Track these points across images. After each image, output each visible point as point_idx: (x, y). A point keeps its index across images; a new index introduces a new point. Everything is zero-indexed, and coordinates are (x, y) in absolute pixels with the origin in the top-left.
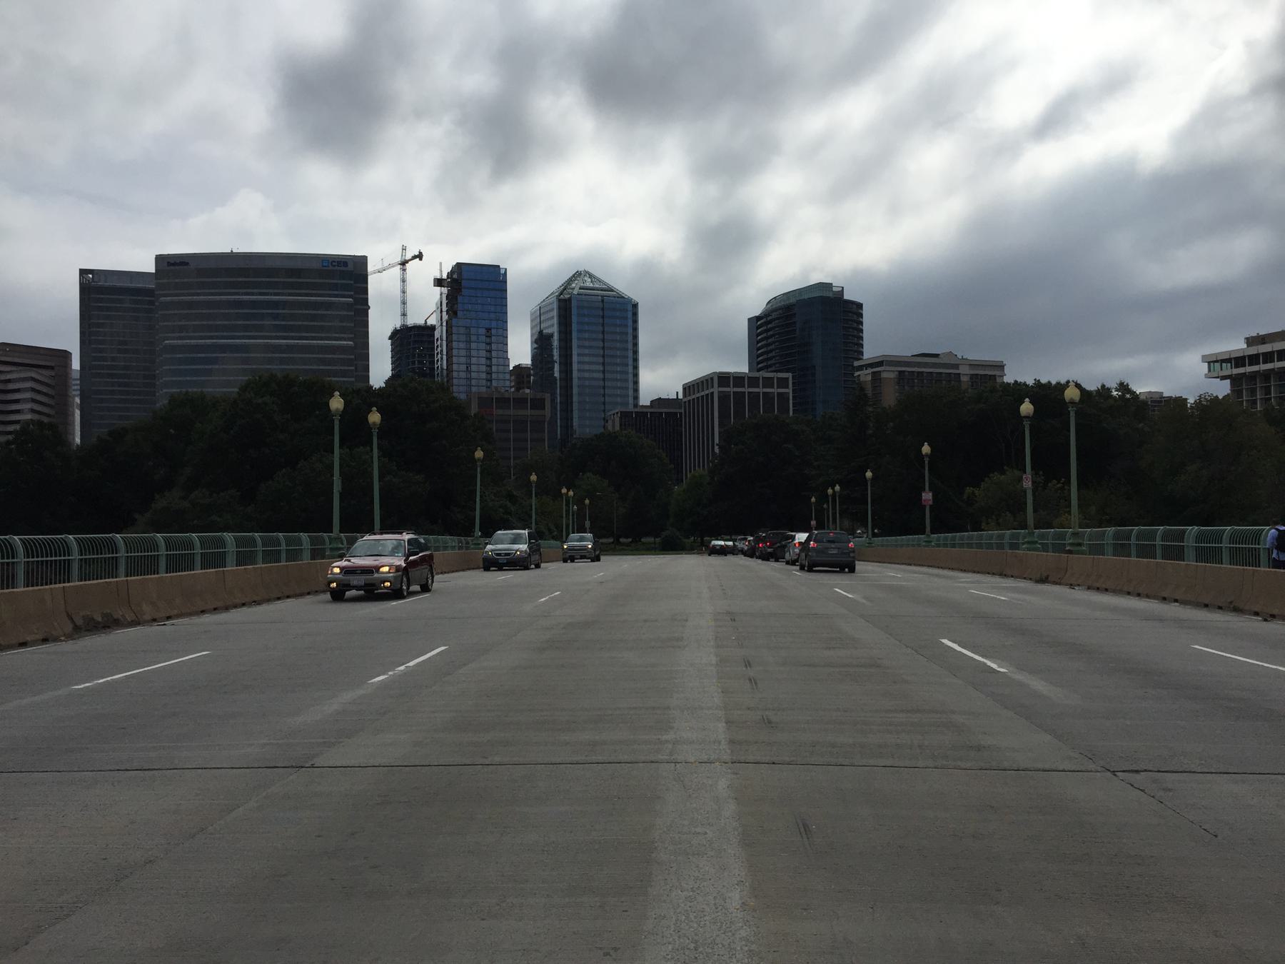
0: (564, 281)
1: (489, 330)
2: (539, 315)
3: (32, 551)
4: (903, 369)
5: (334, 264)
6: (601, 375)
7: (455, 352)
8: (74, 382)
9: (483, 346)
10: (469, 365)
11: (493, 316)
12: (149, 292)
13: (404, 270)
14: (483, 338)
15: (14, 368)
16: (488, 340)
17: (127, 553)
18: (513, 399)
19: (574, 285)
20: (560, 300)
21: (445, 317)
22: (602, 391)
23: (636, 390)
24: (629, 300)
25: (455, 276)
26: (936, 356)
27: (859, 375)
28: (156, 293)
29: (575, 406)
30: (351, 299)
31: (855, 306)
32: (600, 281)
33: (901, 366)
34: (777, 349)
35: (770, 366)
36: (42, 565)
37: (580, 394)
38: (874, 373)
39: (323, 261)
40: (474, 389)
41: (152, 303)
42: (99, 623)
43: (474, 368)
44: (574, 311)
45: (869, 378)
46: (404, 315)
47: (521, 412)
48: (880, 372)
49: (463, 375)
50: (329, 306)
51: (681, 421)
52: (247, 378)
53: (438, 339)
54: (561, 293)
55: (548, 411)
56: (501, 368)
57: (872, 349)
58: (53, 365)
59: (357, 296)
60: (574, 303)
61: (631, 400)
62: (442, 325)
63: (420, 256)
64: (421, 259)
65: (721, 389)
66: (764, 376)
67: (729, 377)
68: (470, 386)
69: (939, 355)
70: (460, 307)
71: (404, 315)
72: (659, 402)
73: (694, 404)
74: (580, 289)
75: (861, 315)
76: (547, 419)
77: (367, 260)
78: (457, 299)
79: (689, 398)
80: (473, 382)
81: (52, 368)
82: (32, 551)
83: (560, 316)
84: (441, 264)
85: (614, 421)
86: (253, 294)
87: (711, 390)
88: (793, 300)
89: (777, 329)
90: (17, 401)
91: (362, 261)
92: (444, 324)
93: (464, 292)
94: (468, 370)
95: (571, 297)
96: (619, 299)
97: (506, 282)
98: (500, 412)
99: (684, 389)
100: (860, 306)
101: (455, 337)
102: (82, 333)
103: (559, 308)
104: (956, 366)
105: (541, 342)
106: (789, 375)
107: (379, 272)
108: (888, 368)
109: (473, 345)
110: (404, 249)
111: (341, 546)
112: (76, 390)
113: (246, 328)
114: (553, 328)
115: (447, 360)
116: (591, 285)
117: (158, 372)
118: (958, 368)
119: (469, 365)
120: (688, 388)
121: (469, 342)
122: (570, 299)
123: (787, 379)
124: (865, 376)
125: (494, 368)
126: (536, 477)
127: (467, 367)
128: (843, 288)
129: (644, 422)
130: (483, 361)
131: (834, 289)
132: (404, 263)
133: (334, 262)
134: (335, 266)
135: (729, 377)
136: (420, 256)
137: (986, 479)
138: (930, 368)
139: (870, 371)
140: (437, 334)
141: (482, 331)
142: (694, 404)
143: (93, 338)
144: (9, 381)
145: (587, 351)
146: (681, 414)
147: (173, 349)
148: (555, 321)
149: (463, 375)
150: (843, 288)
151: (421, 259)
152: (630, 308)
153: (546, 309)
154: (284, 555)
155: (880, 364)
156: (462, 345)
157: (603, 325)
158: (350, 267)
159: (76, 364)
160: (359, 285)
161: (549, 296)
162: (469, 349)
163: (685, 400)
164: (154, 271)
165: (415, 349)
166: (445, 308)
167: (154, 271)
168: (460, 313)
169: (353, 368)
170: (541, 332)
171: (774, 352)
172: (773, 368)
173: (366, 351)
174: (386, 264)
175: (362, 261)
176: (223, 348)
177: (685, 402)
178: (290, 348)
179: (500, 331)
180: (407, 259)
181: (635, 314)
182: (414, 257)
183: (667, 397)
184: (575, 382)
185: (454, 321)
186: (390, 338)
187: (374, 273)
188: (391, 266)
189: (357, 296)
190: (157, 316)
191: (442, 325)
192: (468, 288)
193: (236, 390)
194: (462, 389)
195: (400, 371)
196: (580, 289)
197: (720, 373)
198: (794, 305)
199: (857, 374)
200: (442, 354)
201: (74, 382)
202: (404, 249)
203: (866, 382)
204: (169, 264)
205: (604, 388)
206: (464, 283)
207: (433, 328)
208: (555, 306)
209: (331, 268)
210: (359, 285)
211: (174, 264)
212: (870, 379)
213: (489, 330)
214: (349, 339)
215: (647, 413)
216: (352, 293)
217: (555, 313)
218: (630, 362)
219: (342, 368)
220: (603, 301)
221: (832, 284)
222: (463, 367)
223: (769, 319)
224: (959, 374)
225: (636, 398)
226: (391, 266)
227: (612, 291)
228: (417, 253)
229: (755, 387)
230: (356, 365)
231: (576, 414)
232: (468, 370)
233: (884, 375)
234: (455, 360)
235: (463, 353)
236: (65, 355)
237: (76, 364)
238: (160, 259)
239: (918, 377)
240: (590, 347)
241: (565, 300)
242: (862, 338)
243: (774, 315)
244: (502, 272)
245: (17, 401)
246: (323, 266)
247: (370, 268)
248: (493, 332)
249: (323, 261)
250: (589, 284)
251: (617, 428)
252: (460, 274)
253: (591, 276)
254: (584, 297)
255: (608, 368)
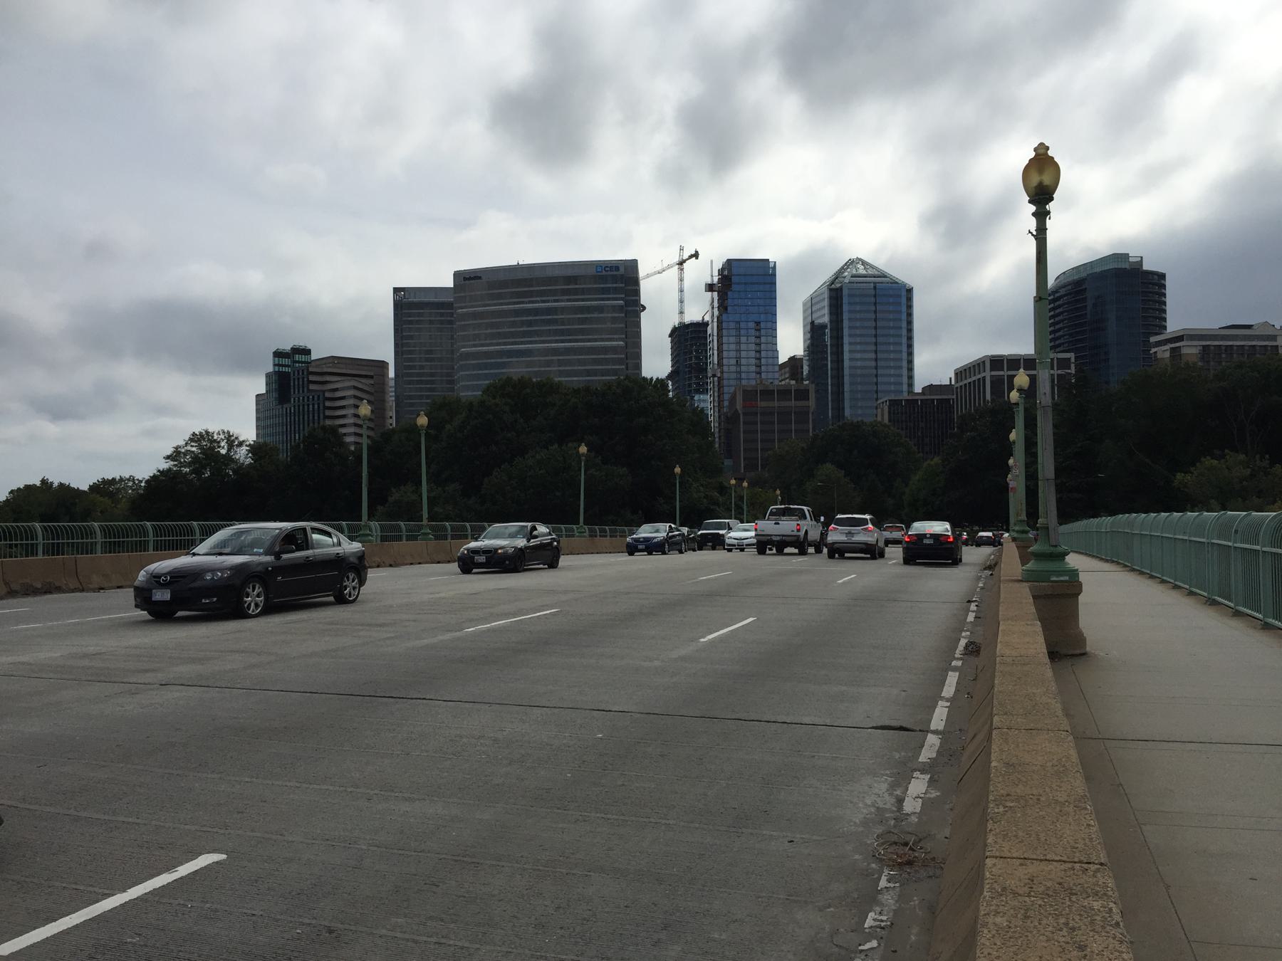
0: (833, 274)
1: (758, 323)
2: (811, 304)
3: (169, 531)
4: (1208, 343)
5: (607, 269)
6: (873, 364)
7: (725, 347)
8: (390, 389)
9: (753, 339)
10: (738, 359)
11: (762, 309)
12: (449, 305)
13: (682, 270)
14: (753, 332)
15: (342, 378)
16: (758, 334)
17: (106, 538)
18: (777, 391)
19: (846, 274)
20: (831, 290)
21: (716, 312)
22: (875, 380)
23: (911, 377)
24: (904, 285)
25: (726, 273)
26: (1249, 327)
27: (1156, 352)
28: (455, 305)
29: (847, 395)
30: (622, 302)
31: (1156, 277)
32: (872, 267)
33: (1206, 340)
34: (1066, 327)
35: (1059, 346)
36: (68, 546)
37: (851, 384)
38: (1173, 349)
39: (597, 266)
40: (744, 382)
41: (452, 315)
42: (37, 588)
43: (743, 361)
44: (845, 300)
45: (1167, 355)
46: (681, 313)
47: (770, 404)
48: (1180, 347)
49: (733, 369)
50: (600, 309)
51: (954, 408)
52: (487, 382)
53: (710, 335)
54: (832, 283)
55: (812, 402)
56: (770, 361)
57: (1175, 322)
58: (372, 374)
59: (627, 298)
60: (845, 292)
61: (905, 388)
62: (712, 321)
63: (696, 255)
64: (697, 258)
65: (994, 373)
66: (1059, 357)
67: (1003, 360)
68: (740, 379)
69: (1252, 325)
70: (729, 302)
71: (681, 313)
72: (930, 389)
73: (961, 391)
74: (852, 277)
75: (1164, 286)
76: (811, 410)
77: (637, 263)
78: (727, 295)
79: (961, 384)
80: (743, 375)
81: (371, 377)
82: (169, 531)
83: (831, 306)
84: (712, 262)
85: (883, 410)
86: (548, 301)
87: (983, 375)
88: (1084, 275)
89: (1066, 306)
90: (343, 407)
91: (632, 265)
92: (715, 320)
93: (734, 287)
94: (738, 364)
95: (842, 286)
96: (894, 285)
97: (775, 275)
98: (764, 404)
99: (956, 374)
100: (1163, 276)
101: (725, 332)
102: (396, 345)
103: (831, 298)
104: (1274, 338)
105: (815, 333)
106: (1071, 356)
107: (659, 273)
108: (1190, 343)
109: (743, 339)
110: (682, 249)
111: (368, 532)
112: (392, 392)
113: (524, 334)
114: (824, 318)
115: (718, 354)
116: (864, 272)
117: (456, 377)
118: (1276, 341)
119: (738, 359)
120: (960, 374)
121: (739, 336)
122: (841, 289)
123: (1069, 359)
124: (1163, 352)
125: (763, 361)
126: (679, 469)
127: (737, 361)
128: (1142, 257)
129: (914, 410)
130: (753, 354)
131: (1131, 260)
132: (681, 263)
133: (607, 267)
134: (608, 271)
135: (1003, 360)
136: (696, 255)
137: (1198, 464)
138: (1242, 340)
139: (1168, 347)
140: (709, 329)
141: (752, 325)
142: (961, 391)
143: (405, 349)
144: (336, 390)
145: (858, 340)
146: (953, 399)
147: (468, 356)
148: (826, 311)
149: (733, 369)
150: (1142, 257)
151: (697, 258)
152: (904, 293)
153: (818, 299)
154: (404, 538)
155: (1180, 338)
156: (732, 339)
157: (875, 312)
158: (622, 271)
159: (392, 374)
160: (630, 288)
161: (821, 286)
162: (739, 343)
163: (958, 385)
164: (452, 286)
165: (692, 345)
166: (716, 304)
167: (452, 286)
168: (729, 308)
169: (623, 367)
170: (812, 323)
171: (1062, 331)
172: (1061, 349)
173: (636, 350)
174: (665, 265)
175: (632, 265)
176: (510, 354)
177: (957, 388)
178: (568, 351)
179: (769, 325)
180: (684, 258)
181: (909, 299)
182: (691, 257)
183: (939, 384)
184: (846, 372)
185: (724, 317)
186: (670, 336)
187: (648, 276)
188: (669, 267)
189: (627, 298)
190: (454, 326)
191: (712, 321)
192: (738, 284)
193: (480, 393)
194: (732, 382)
195: (678, 367)
196: (852, 277)
197: (993, 356)
198: (1086, 279)
199: (1153, 350)
200: (713, 350)
201: (390, 389)
202: (682, 249)
203: (1164, 359)
204: (465, 279)
205: (876, 376)
206: (734, 279)
207: (707, 324)
208: (826, 295)
209: (604, 273)
210: (630, 288)
211: (470, 279)
212: (1168, 356)
213: (758, 323)
214: (621, 339)
215: (917, 400)
216: (623, 296)
217: (826, 303)
218: (904, 348)
219: (614, 367)
220: (875, 288)
221: (1128, 254)
222: (733, 362)
223: (1057, 295)
224: (1277, 346)
225: (911, 385)
226: (669, 267)
227: (885, 277)
228: (693, 253)
229: (1032, 370)
230: (627, 364)
231: (847, 404)
232: (738, 364)
233: (1184, 351)
234: (725, 354)
235: (733, 347)
236: (382, 365)
237: (392, 374)
238: (458, 275)
239: (1226, 351)
240: (861, 336)
241: (837, 289)
242: (1165, 311)
243: (1062, 292)
244: (771, 265)
245: (343, 407)
246: (597, 272)
247: (642, 273)
248: (762, 325)
249: (597, 266)
250: (862, 270)
251: (886, 420)
252: (730, 270)
253: (864, 263)
254: (855, 285)
255: (880, 356)
